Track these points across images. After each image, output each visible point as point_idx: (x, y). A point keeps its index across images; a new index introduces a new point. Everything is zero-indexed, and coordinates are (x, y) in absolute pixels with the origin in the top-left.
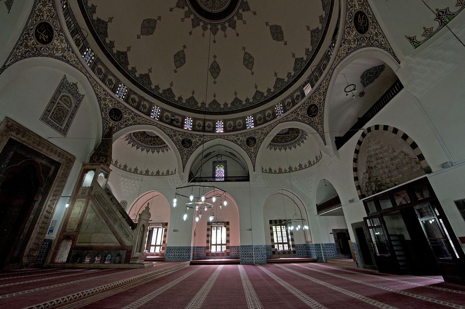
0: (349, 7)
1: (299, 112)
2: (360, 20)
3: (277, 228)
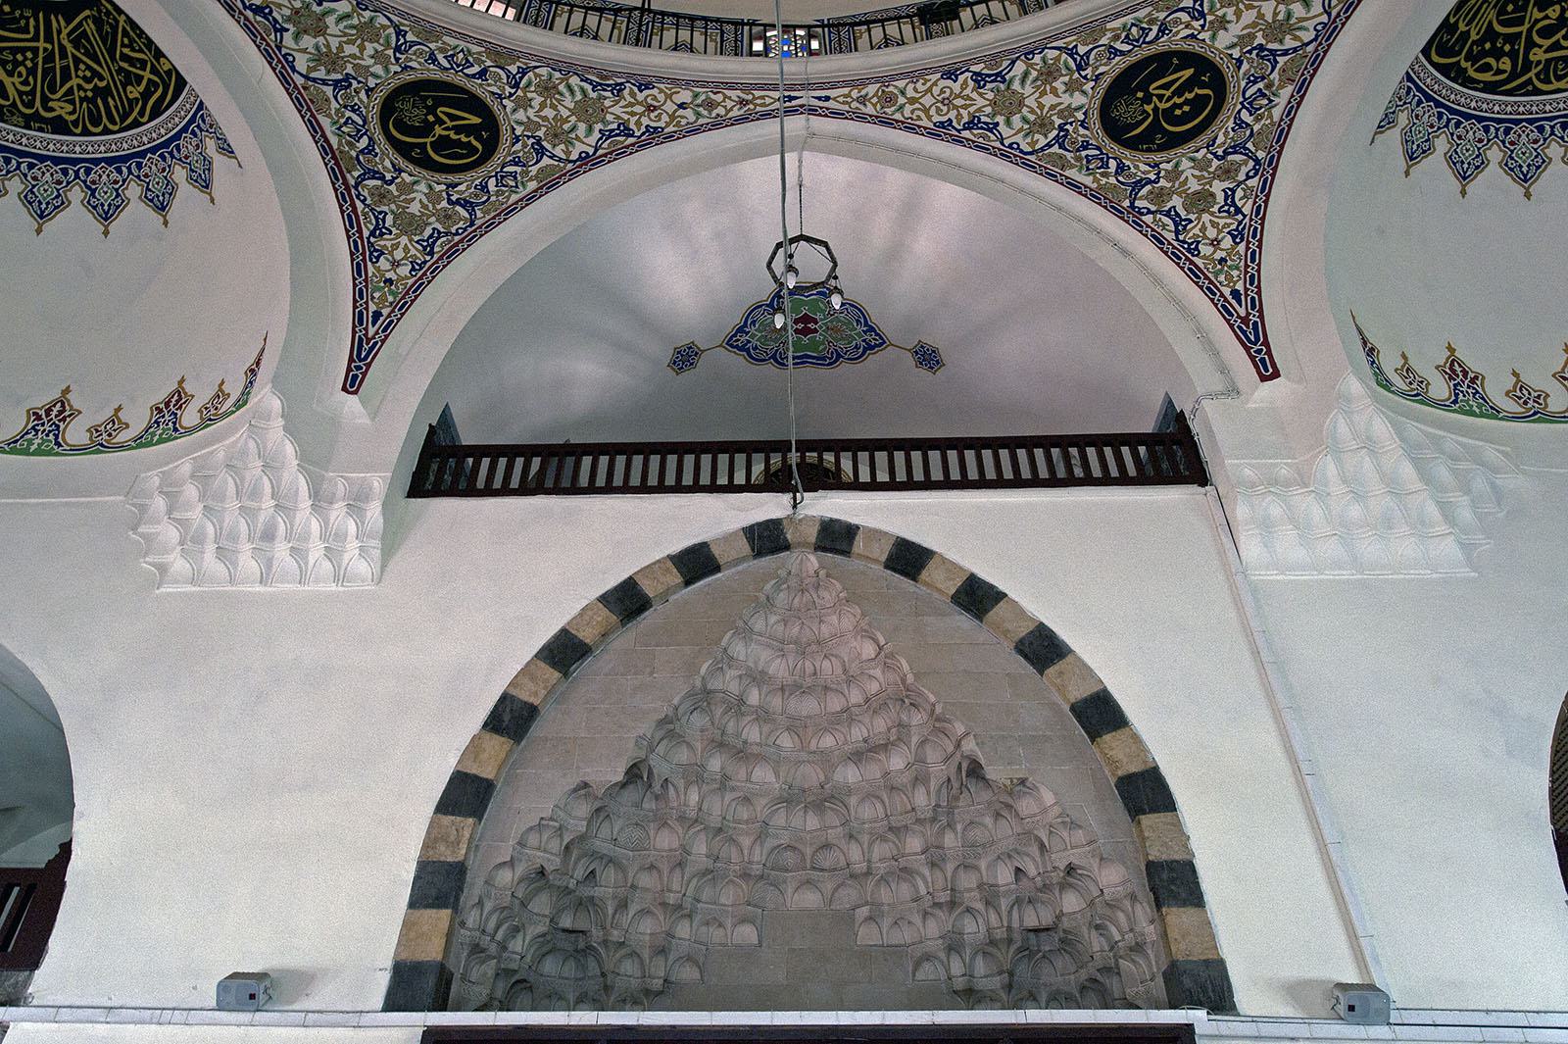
1: (330, 20)
3: (1035, 918)
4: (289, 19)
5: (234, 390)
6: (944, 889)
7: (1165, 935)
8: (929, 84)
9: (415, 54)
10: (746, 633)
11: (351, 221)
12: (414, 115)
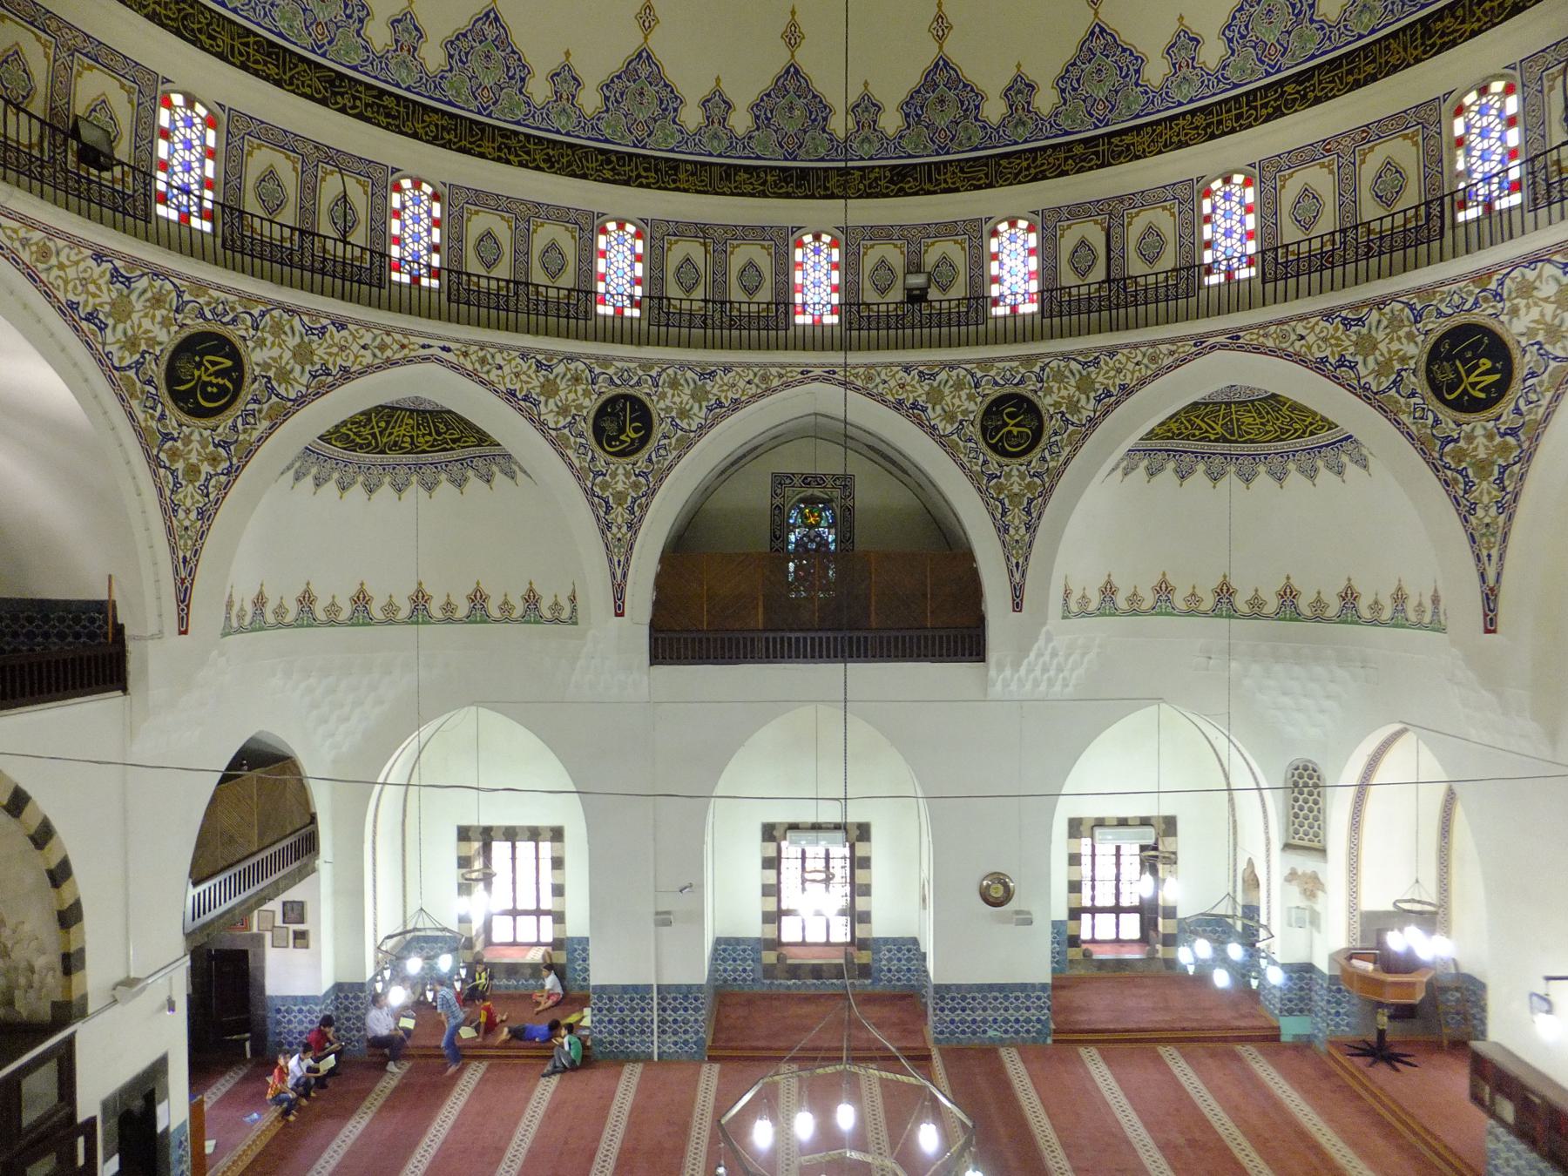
2: (214, 364)
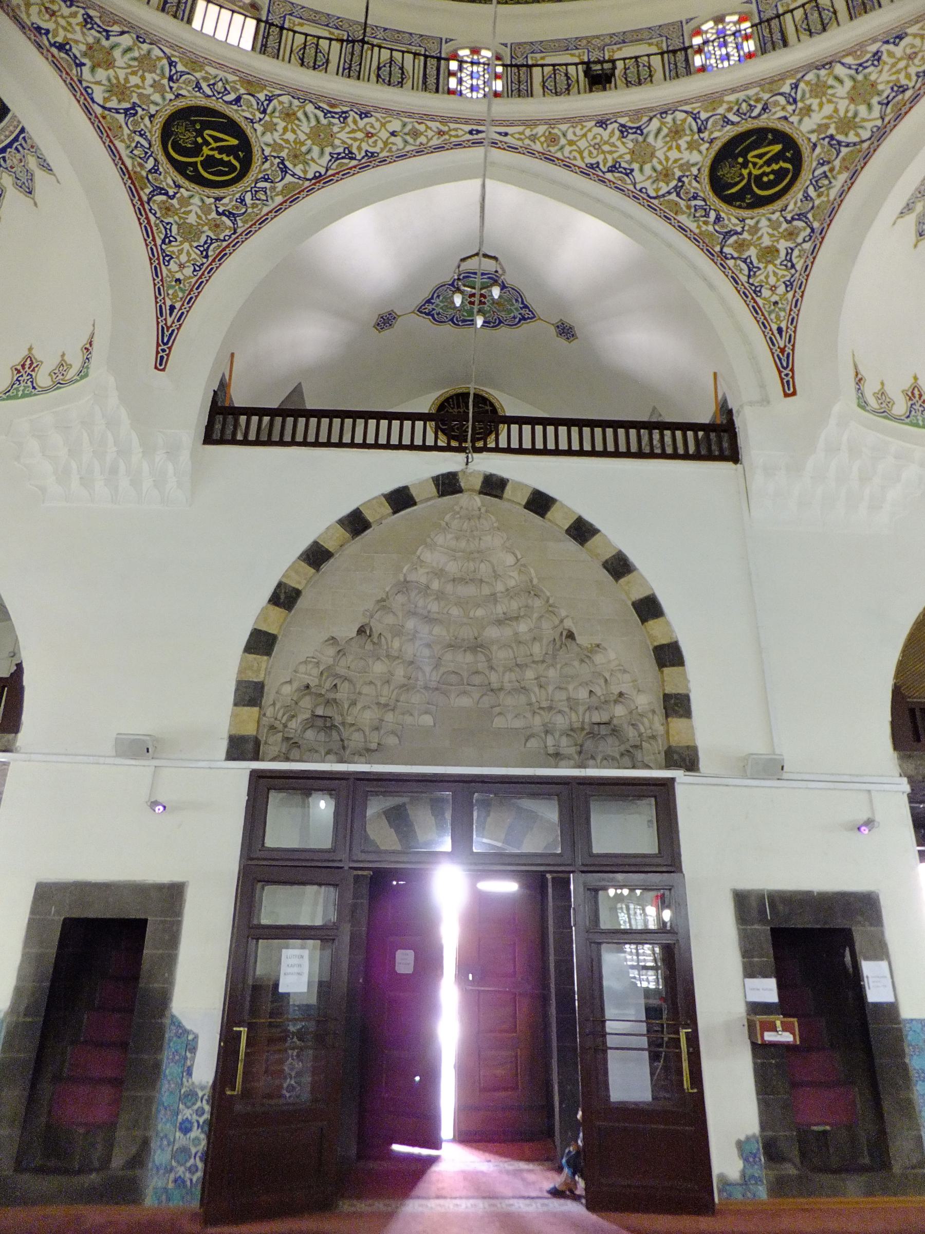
0: (786, 89)
1: (117, 53)
2: (760, 156)
4: (85, 54)
5: (76, 362)
6: (547, 700)
7: (667, 732)
8: (585, 130)
9: (184, 83)
10: (432, 547)
11: (148, 231)
12: (187, 138)
